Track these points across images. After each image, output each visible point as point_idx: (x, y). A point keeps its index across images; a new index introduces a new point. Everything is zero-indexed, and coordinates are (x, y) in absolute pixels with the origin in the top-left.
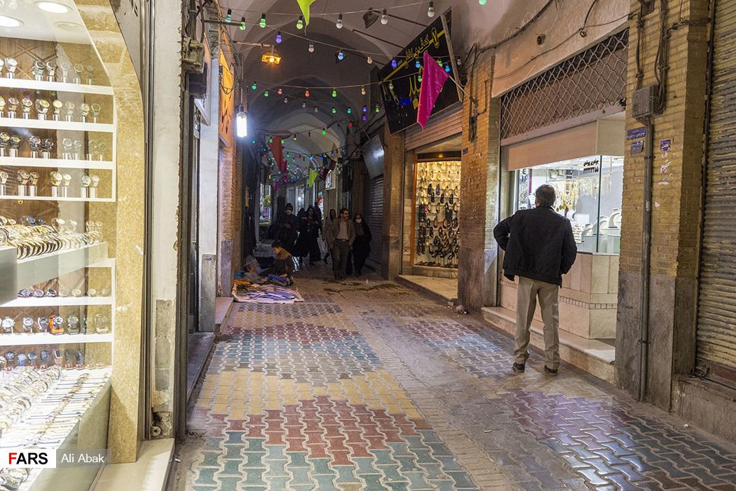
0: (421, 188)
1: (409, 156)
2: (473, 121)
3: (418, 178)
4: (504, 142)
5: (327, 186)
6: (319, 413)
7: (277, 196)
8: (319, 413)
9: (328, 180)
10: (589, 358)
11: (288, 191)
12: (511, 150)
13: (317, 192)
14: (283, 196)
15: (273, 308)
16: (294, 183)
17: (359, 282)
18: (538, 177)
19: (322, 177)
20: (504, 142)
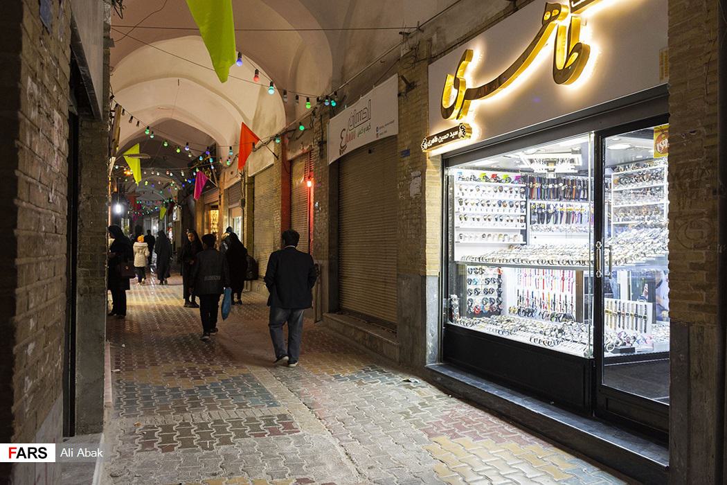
0: (213, 224)
1: (207, 207)
2: (220, 197)
3: (212, 218)
4: (230, 207)
5: (174, 219)
6: (266, 433)
7: (136, 225)
8: (266, 433)
9: (175, 215)
10: (224, 312)
11: (144, 221)
12: (233, 210)
13: (168, 222)
14: (140, 225)
15: (535, 194)
16: (151, 215)
17: (508, 309)
18: (102, 64)
19: (170, 212)
20: (230, 207)
